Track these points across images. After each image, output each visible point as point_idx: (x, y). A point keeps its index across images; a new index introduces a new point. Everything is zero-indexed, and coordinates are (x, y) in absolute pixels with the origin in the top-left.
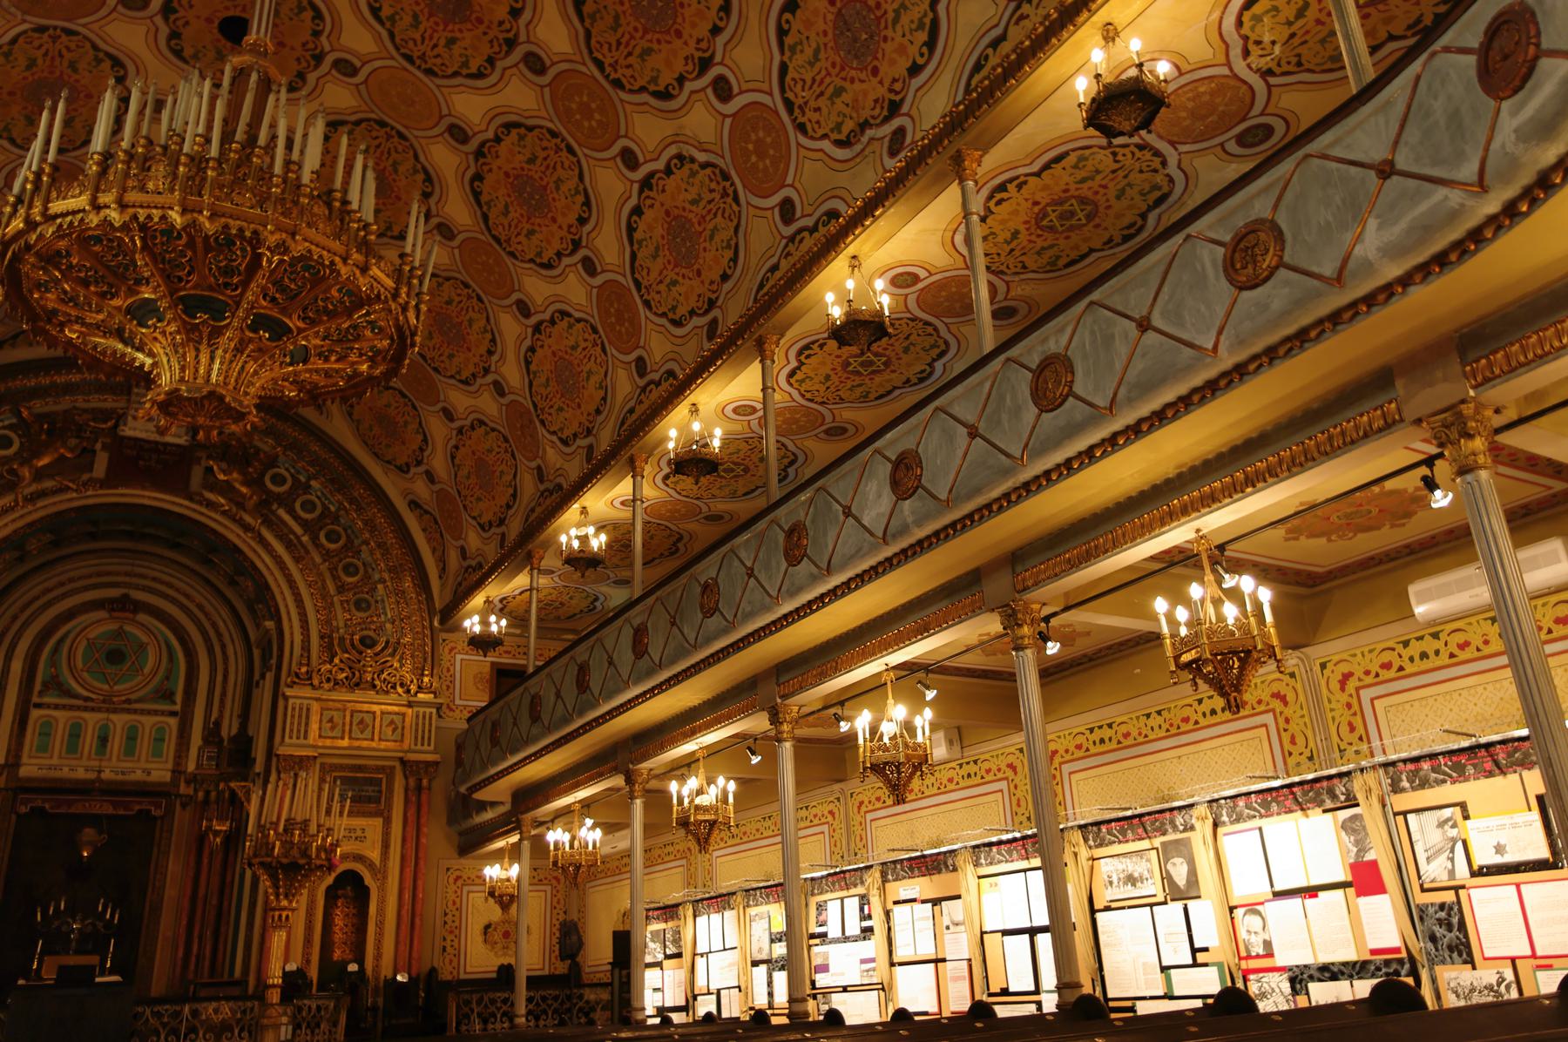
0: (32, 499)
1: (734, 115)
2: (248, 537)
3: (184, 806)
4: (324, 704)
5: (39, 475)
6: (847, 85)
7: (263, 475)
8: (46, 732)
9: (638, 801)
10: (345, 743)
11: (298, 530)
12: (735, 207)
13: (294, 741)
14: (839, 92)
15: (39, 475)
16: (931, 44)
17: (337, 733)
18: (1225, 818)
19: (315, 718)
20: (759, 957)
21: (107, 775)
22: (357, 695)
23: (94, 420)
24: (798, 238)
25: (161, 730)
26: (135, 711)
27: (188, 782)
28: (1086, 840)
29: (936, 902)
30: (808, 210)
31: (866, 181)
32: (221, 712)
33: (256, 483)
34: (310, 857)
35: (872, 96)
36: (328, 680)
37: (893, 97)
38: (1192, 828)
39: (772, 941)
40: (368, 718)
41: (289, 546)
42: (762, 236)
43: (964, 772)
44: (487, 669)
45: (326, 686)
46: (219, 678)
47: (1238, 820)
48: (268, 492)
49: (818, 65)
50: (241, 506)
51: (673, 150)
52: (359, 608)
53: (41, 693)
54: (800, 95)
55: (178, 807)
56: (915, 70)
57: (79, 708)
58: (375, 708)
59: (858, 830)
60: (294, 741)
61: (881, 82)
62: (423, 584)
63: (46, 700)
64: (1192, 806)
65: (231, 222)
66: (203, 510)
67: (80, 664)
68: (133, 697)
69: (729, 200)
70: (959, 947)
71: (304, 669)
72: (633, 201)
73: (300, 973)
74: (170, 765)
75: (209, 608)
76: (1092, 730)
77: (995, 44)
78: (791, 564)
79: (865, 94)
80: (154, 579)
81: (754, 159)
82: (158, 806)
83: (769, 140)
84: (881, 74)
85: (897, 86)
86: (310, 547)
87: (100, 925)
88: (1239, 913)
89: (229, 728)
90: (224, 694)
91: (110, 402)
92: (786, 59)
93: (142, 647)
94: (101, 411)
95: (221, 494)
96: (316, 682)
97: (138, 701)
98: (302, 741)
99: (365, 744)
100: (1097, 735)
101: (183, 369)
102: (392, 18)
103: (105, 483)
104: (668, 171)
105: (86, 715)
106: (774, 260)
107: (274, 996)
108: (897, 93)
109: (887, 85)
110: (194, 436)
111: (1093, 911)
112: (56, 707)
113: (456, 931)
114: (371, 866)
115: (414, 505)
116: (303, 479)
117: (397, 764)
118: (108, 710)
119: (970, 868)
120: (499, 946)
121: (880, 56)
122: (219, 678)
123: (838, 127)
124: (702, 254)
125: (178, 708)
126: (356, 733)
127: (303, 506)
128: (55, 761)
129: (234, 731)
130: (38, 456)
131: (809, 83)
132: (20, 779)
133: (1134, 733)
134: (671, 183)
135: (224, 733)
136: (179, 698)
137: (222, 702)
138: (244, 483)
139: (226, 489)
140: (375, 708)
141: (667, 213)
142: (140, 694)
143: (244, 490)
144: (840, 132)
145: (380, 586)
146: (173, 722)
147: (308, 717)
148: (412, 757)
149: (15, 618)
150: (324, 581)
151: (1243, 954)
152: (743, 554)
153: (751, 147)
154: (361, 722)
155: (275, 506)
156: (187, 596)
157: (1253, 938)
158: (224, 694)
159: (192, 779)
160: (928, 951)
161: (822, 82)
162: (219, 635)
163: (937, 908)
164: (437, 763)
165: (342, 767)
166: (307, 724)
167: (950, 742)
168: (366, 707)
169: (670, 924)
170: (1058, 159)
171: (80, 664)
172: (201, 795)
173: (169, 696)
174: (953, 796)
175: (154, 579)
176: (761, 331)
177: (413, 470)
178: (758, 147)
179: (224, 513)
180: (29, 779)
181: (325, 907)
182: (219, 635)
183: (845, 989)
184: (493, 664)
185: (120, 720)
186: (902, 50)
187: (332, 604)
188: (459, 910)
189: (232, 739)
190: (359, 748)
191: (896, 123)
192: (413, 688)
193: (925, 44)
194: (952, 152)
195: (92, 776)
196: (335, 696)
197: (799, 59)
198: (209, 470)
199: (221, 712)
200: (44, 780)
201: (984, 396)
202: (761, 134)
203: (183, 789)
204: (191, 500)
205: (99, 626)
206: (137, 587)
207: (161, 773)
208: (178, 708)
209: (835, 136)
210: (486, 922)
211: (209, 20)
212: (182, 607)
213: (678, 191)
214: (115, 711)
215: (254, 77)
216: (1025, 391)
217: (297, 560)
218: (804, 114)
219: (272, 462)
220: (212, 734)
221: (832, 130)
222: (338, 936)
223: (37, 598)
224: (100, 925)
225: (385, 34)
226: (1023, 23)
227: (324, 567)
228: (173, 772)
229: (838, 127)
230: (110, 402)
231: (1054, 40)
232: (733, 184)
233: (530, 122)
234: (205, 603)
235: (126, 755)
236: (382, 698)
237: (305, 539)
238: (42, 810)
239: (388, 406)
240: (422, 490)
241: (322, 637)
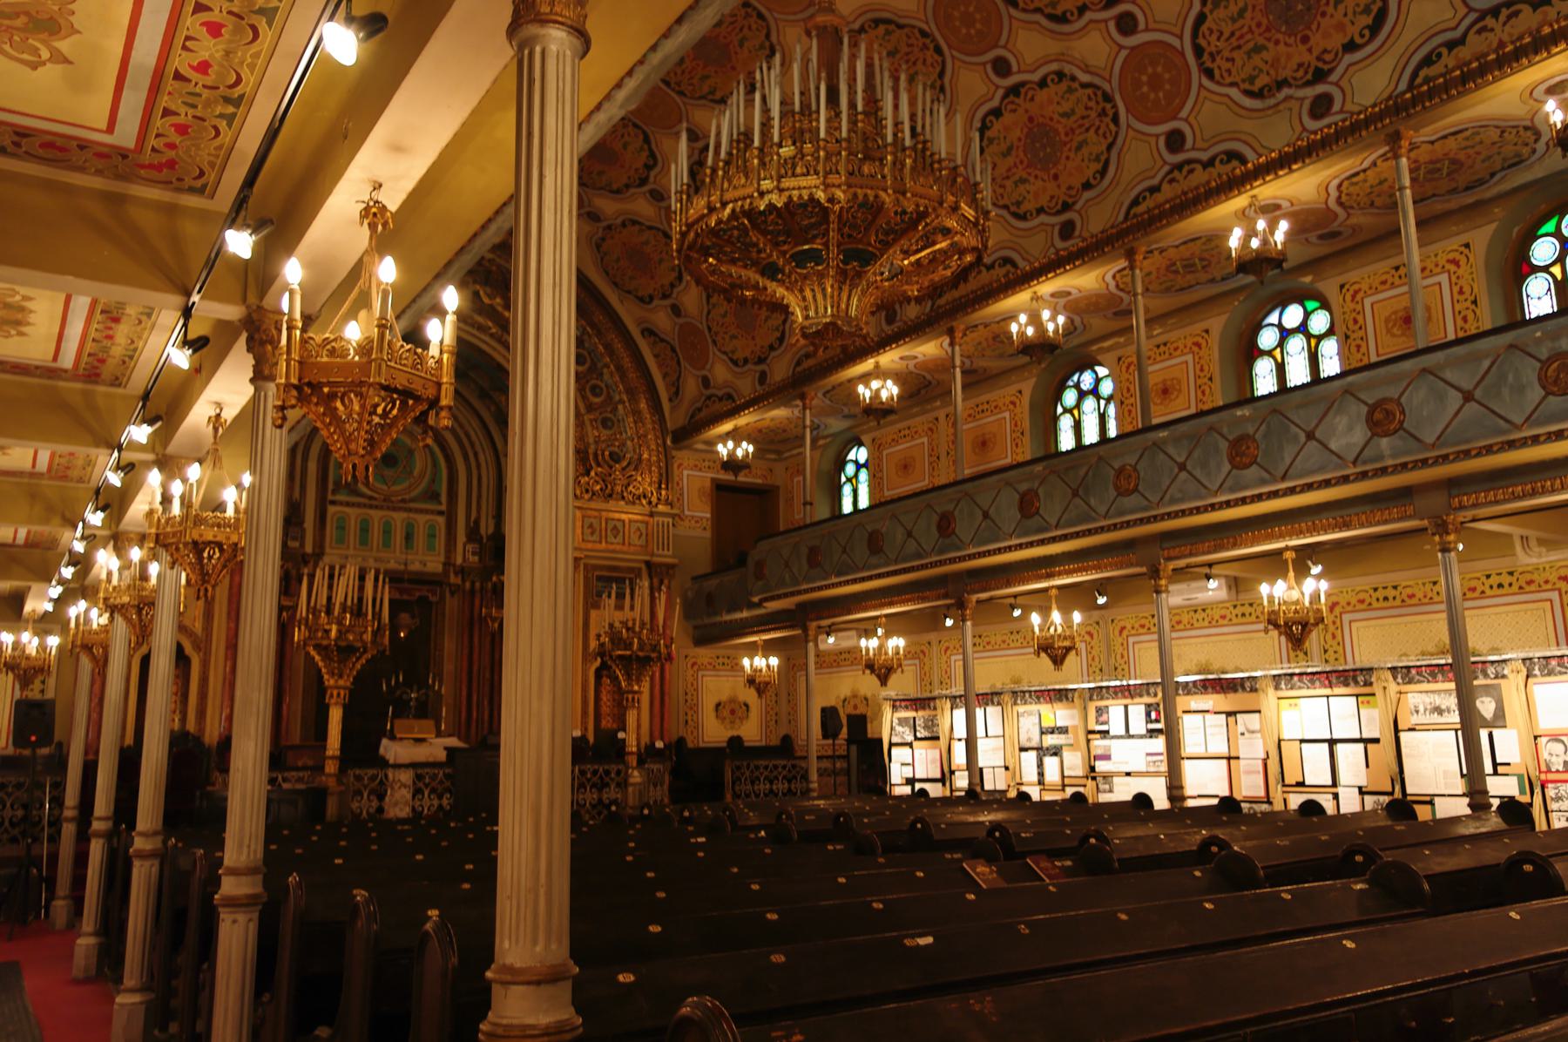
1: (1132, 49)
3: (452, 594)
6: (1270, 45)
8: (342, 527)
9: (969, 623)
12: (1112, 126)
14: (1258, 49)
16: (1375, 28)
17: (595, 538)
18: (1537, 672)
20: (1028, 745)
21: (412, 568)
22: (612, 505)
24: (1186, 168)
25: (432, 527)
26: (410, 510)
27: (456, 574)
28: (1395, 678)
29: (1229, 714)
30: (1199, 144)
31: (1279, 134)
32: (479, 511)
35: (1296, 60)
37: (1320, 65)
38: (1504, 677)
39: (1042, 733)
40: (619, 525)
42: (1141, 156)
43: (1239, 610)
44: (708, 484)
45: (586, 496)
47: (1549, 674)
49: (1241, 22)
51: (1054, 67)
52: (605, 426)
53: (334, 492)
54: (1211, 43)
55: (448, 595)
56: (1351, 47)
57: (365, 506)
58: (624, 516)
59: (1119, 650)
61: (1310, 50)
62: (656, 406)
63: (340, 498)
64: (1504, 661)
65: (859, 191)
69: (1108, 120)
70: (1252, 750)
72: (995, 103)
73: (584, 738)
74: (442, 559)
76: (1375, 590)
77: (1451, 45)
78: (1234, 466)
79: (1289, 57)
81: (1145, 89)
82: (434, 594)
83: (1167, 76)
84: (1312, 42)
85: (1328, 57)
88: (1543, 740)
89: (487, 528)
90: (479, 496)
92: (1206, 10)
97: (412, 500)
99: (618, 547)
100: (1380, 594)
101: (806, 308)
104: (1043, 83)
105: (372, 512)
106: (1155, 181)
107: (633, 761)
108: (1325, 62)
109: (1315, 54)
111: (1397, 731)
112: (348, 504)
113: (695, 707)
115: (648, 332)
117: (643, 566)
119: (1271, 691)
121: (1314, 27)
123: (1252, 79)
124: (1063, 161)
125: (443, 508)
126: (611, 539)
129: (491, 530)
131: (1226, 35)
133: (1420, 595)
134: (1042, 95)
135: (483, 531)
136: (444, 498)
140: (624, 516)
141: (1031, 119)
142: (414, 494)
144: (1252, 83)
145: (620, 407)
146: (441, 520)
148: (656, 559)
151: (1543, 768)
152: (1171, 450)
153: (1144, 78)
154: (615, 528)
157: (1554, 759)
158: (479, 496)
159: (462, 571)
160: (1224, 750)
161: (1242, 37)
163: (1231, 719)
164: (673, 566)
167: (1229, 588)
168: (617, 516)
169: (921, 713)
170: (1461, 131)
172: (468, 585)
173: (435, 497)
174: (1225, 630)
176: (1135, 244)
177: (656, 302)
178: (1154, 80)
179: (492, 335)
183: (1128, 774)
184: (713, 480)
185: (399, 517)
186: (1340, 27)
188: (696, 690)
189: (489, 538)
190: (614, 551)
191: (1320, 88)
192: (654, 500)
193: (1368, 27)
194: (1391, 130)
196: (593, 505)
197: (1221, 13)
199: (479, 511)
201: (1482, 372)
202: (1159, 69)
203: (453, 579)
207: (434, 565)
208: (443, 508)
209: (1247, 86)
210: (716, 701)
213: (1049, 104)
214: (394, 509)
216: (1533, 377)
218: (1214, 60)
220: (473, 534)
221: (1244, 81)
222: (605, 709)
226: (1484, 35)
228: (445, 564)
229: (1252, 79)
231: (1525, 61)
232: (1115, 106)
233: (902, 21)
236: (630, 508)
239: (647, 243)
240: (662, 320)
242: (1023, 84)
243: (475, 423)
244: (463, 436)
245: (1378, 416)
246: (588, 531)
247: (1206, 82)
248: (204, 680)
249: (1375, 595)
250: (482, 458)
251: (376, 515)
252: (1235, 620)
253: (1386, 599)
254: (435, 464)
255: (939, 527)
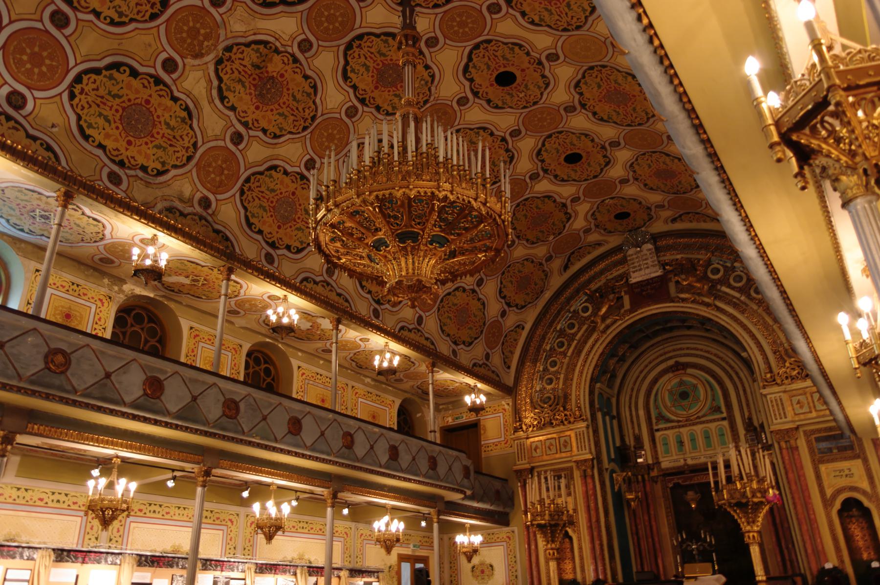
0: (604, 332)
2: (709, 310)
4: (790, 393)
5: (604, 318)
7: (706, 273)
10: (814, 414)
11: (737, 295)
13: (779, 421)
15: (604, 318)
19: (787, 404)
21: (690, 462)
23: (617, 281)
25: (721, 429)
26: (703, 422)
32: (750, 411)
33: (704, 278)
34: (747, 497)
36: (787, 378)
41: (735, 306)
45: (786, 381)
46: (741, 393)
48: (712, 281)
50: (699, 294)
57: (676, 427)
60: (779, 421)
63: (660, 426)
66: (682, 305)
67: (669, 404)
68: (700, 414)
71: (769, 376)
75: (721, 355)
80: (688, 348)
86: (748, 301)
87: (706, 545)
91: (621, 270)
93: (695, 386)
94: (619, 276)
95: (687, 292)
96: (779, 381)
98: (784, 420)
102: (541, 20)
103: (632, 310)
110: (664, 269)
112: (666, 429)
114: (864, 493)
116: (729, 265)
118: (690, 425)
120: (480, 578)
122: (741, 393)
125: (725, 415)
127: (735, 281)
128: (675, 457)
130: (600, 309)
132: (663, 470)
137: (748, 405)
138: (697, 281)
139: (689, 289)
143: (698, 285)
146: (725, 423)
147: (782, 404)
149: (632, 389)
150: (763, 318)
154: (565, 441)
155: (719, 287)
156: (708, 352)
162: (732, 368)
165: (819, 431)
166: (783, 409)
171: (669, 404)
173: (718, 409)
175: (688, 348)
179: (693, 302)
180: (667, 469)
181: (842, 524)
182: (732, 368)
185: (698, 428)
187: (773, 330)
195: (682, 462)
198: (677, 282)
199: (750, 411)
200: (674, 468)
204: (673, 302)
205: (669, 382)
206: (681, 356)
211: (492, 85)
212: (707, 359)
214: (694, 424)
215: (411, 116)
217: (743, 312)
219: (709, 263)
223: (638, 377)
224: (706, 545)
225: (546, 29)
227: (760, 311)
230: (621, 270)
234: (718, 353)
235: (708, 447)
237: (743, 298)
238: (678, 483)
241: (775, 353)
242: (472, 90)
243: (730, 354)
244: (723, 364)
245: (60, 358)
246: (797, 407)
247: (200, 143)
248: (580, 549)
249: (52, 497)
250: (742, 375)
251: (684, 431)
252: (148, 515)
253: (58, 501)
254: (712, 389)
255: (352, 442)
